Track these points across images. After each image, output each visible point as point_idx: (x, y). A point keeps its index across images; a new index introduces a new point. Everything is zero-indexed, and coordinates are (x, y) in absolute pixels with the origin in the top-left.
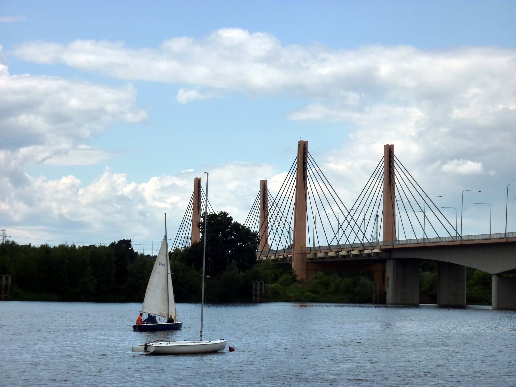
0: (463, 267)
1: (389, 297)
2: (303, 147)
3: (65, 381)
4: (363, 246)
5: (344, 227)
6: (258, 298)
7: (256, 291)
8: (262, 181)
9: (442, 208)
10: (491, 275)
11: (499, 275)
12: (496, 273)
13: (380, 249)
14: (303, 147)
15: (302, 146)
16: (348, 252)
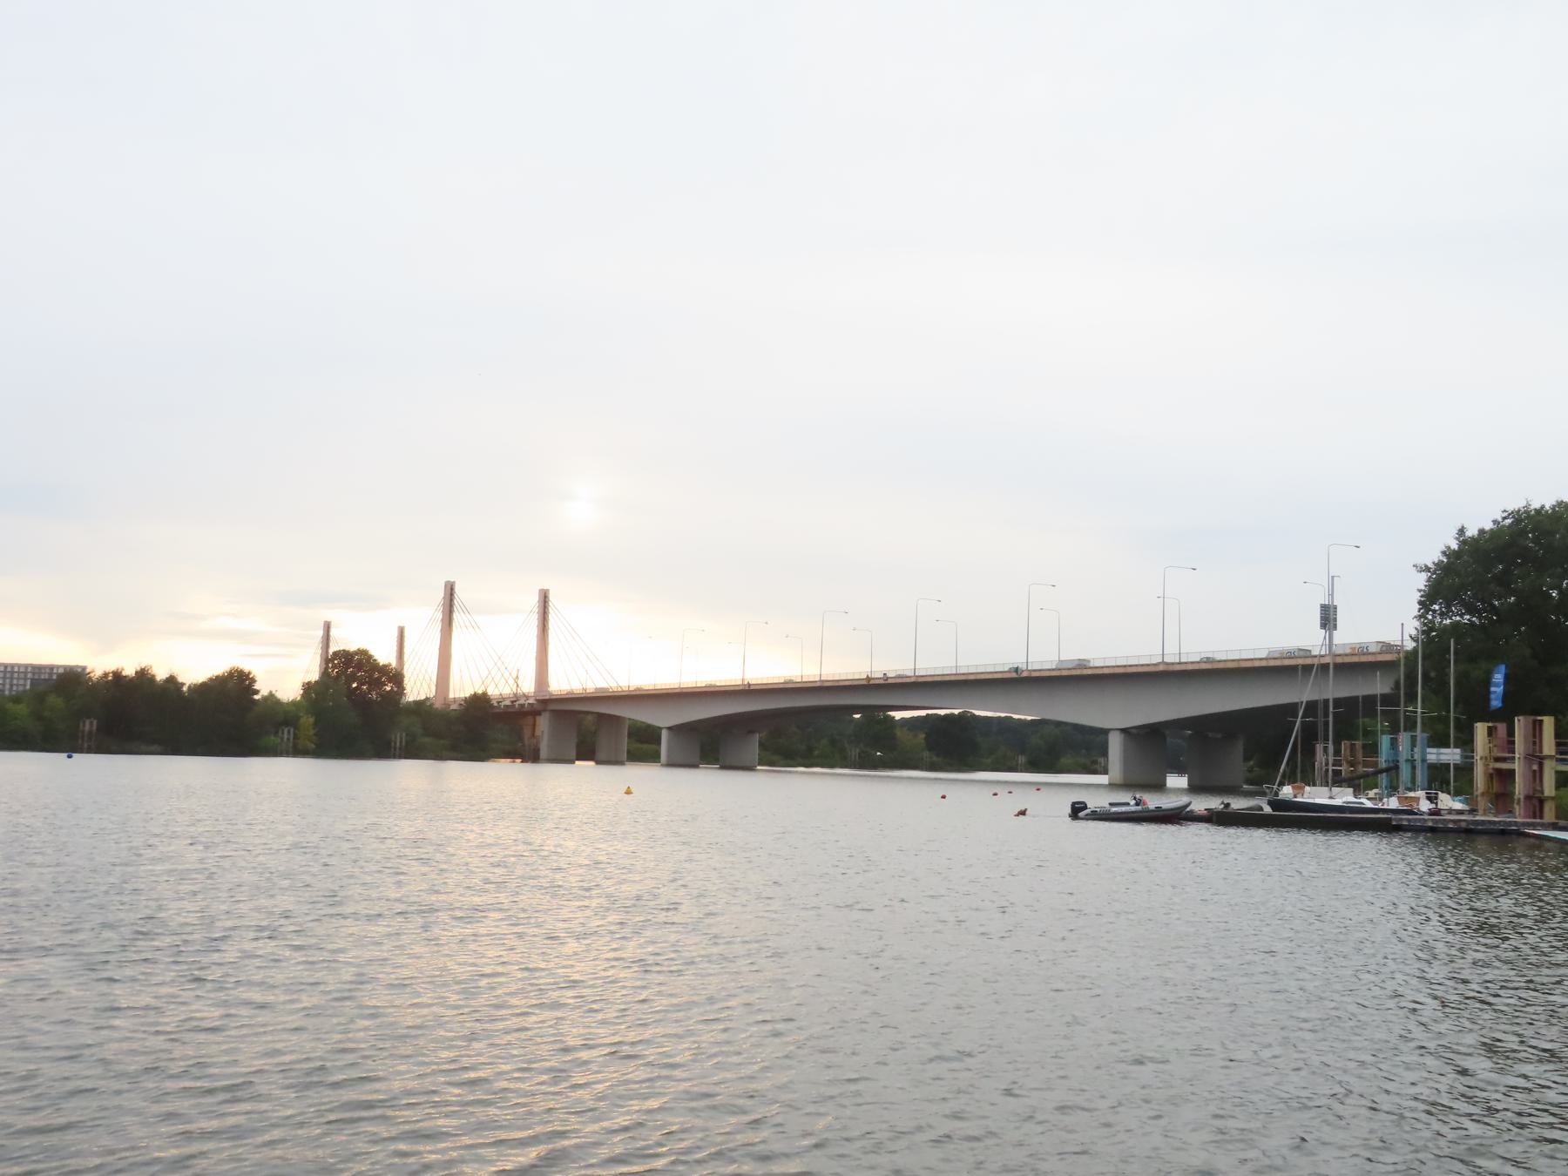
0: (624, 718)
1: (543, 753)
2: (450, 590)
3: (963, 1111)
4: (516, 697)
5: (493, 673)
6: (398, 752)
7: (395, 743)
8: (541, 591)
9: (1358, 547)
10: (660, 729)
11: (669, 728)
12: (667, 726)
13: (536, 700)
14: (450, 590)
15: (449, 587)
16: (512, 702)
